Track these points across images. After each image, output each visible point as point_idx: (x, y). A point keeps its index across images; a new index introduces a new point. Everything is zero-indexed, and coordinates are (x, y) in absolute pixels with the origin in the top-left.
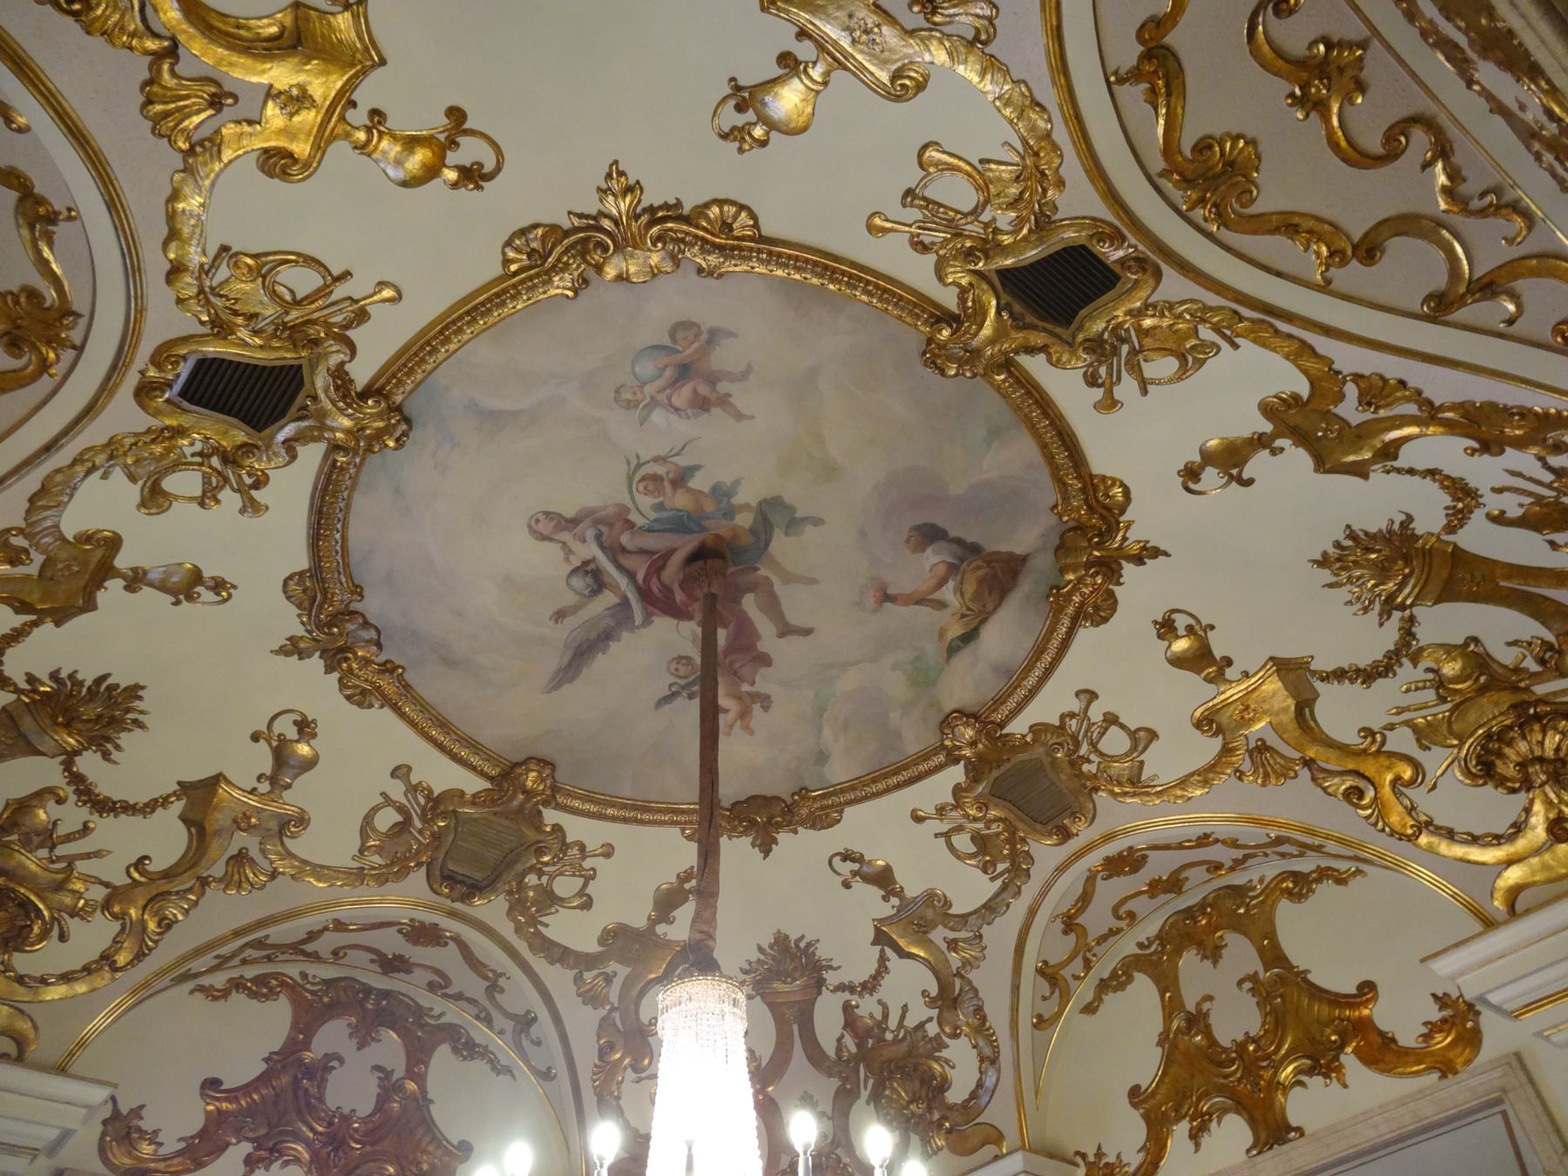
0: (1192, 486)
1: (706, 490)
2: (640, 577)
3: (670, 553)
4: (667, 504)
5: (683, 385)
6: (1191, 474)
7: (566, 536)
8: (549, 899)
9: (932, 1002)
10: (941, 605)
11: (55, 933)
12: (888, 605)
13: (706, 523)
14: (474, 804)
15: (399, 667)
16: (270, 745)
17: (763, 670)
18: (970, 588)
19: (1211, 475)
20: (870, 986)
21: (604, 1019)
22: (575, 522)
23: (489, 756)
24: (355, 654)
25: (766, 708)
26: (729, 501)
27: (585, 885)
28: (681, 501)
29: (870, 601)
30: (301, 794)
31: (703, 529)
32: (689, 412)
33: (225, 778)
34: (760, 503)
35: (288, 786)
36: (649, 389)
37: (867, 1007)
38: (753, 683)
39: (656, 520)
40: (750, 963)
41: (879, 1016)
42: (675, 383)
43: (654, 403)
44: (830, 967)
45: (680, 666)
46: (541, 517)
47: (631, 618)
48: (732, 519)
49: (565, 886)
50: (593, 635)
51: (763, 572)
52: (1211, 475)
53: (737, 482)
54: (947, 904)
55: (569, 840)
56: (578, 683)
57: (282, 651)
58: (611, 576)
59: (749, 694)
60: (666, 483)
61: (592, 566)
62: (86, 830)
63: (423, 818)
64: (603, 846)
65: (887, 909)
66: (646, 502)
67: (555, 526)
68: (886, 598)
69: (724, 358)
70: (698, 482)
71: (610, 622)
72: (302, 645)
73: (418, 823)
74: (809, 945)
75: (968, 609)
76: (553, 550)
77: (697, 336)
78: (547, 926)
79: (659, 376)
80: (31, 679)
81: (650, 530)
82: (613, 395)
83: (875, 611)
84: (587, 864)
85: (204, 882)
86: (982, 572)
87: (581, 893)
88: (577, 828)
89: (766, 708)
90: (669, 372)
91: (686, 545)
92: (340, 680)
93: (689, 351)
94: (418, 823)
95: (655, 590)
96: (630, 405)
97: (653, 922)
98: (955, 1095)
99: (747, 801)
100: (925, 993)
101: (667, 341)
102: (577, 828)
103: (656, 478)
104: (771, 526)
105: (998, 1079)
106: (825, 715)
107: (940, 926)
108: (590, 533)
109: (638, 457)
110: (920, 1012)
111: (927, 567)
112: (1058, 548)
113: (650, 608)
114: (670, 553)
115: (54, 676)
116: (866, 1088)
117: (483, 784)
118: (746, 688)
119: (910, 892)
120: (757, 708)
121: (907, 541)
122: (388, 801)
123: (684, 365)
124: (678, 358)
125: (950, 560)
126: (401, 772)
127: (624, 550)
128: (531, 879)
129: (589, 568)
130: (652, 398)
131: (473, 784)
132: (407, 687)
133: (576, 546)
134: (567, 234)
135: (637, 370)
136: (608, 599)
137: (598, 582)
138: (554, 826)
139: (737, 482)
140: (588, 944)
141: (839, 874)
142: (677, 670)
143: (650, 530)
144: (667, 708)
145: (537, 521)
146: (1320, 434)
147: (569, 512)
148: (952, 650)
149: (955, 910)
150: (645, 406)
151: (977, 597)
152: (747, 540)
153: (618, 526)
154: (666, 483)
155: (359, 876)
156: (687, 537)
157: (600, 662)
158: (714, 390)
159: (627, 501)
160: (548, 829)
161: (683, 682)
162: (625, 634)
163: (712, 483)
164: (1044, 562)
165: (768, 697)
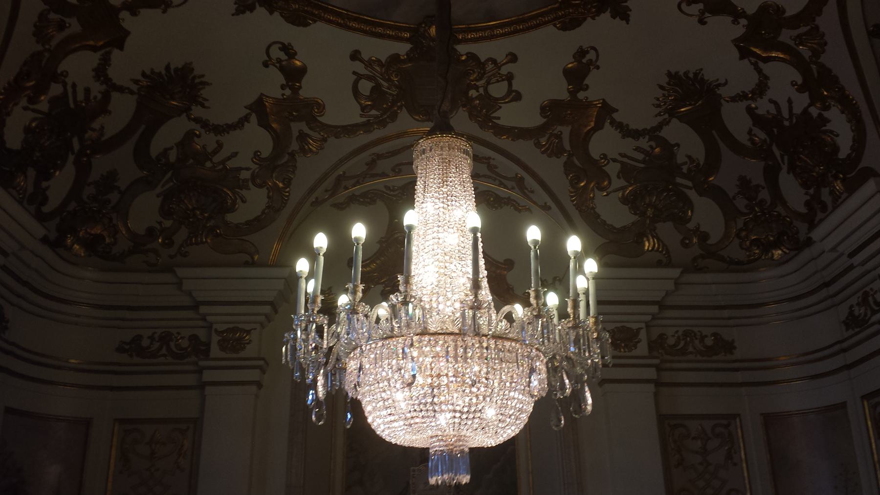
8: (491, 103)
9: (801, 89)
11: (239, 200)
16: (276, 67)
20: (761, 89)
21: (565, 163)
27: (510, 85)
30: (308, 89)
33: (263, 94)
35: (300, 87)
37: (763, 107)
40: (658, 99)
41: (773, 111)
44: (719, 85)
49: (498, 90)
54: (780, 10)
55: (483, 60)
62: (220, 146)
65: (739, 30)
74: (696, 74)
78: (499, 118)
80: (136, 82)
84: (504, 71)
85: (292, 155)
87: (510, 90)
88: (484, 50)
97: (573, 93)
98: (844, 153)
100: (794, 84)
102: (484, 50)
105: (251, 243)
107: (304, 122)
110: (801, 101)
115: (144, 75)
116: (784, 164)
117: (407, 46)
119: (305, 93)
128: (473, 93)
131: (402, 48)
138: (467, 54)
140: (536, 120)
141: (691, 15)
149: (789, 13)
155: (367, 127)
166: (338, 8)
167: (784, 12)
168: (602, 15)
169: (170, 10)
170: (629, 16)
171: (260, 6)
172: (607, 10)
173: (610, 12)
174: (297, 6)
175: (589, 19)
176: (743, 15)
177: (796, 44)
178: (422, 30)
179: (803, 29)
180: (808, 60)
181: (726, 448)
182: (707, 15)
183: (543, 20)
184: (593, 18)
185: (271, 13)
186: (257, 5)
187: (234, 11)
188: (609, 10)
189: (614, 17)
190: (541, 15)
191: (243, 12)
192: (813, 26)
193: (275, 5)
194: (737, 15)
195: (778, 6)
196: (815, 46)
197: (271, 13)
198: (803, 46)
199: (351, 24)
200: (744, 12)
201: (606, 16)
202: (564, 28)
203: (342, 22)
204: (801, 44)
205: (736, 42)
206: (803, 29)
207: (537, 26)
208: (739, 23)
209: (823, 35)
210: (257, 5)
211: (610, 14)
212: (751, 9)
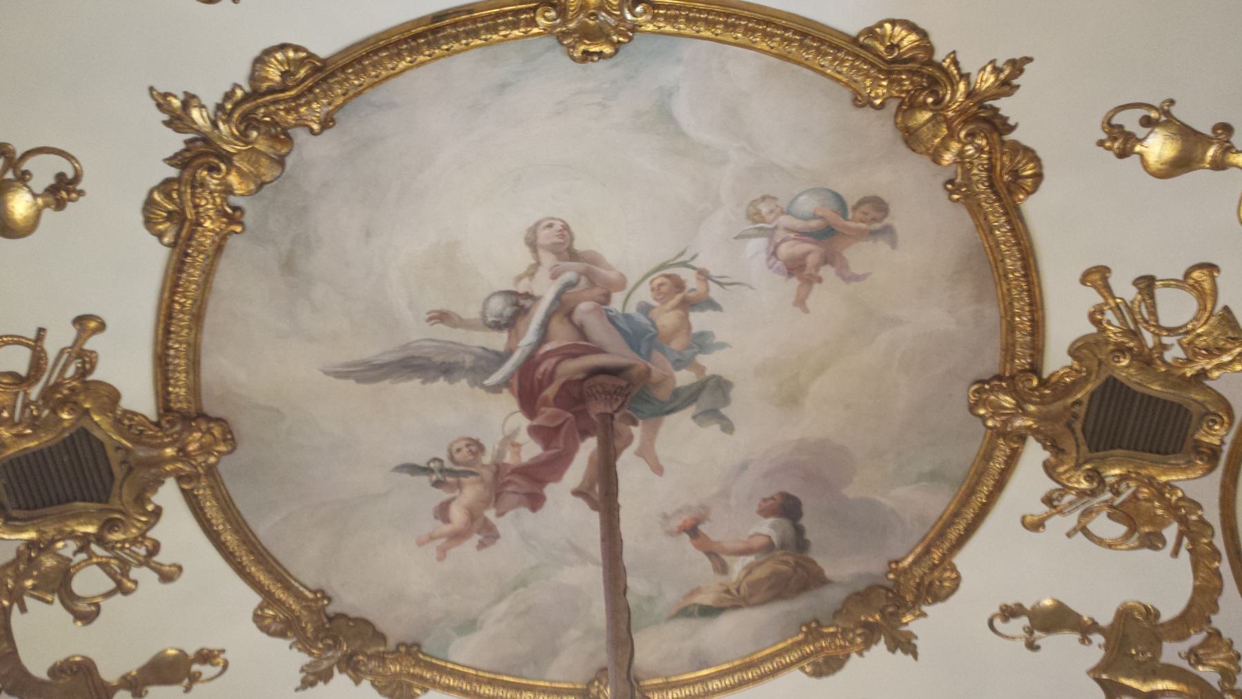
0: (998, 623)
1: (695, 330)
2: (548, 347)
3: (599, 350)
4: (654, 314)
5: (811, 243)
6: (1009, 613)
7: (548, 259)
10: (722, 569)
12: (686, 537)
13: (657, 355)
14: (118, 422)
15: (240, 223)
17: (525, 512)
18: (759, 573)
19: (1018, 625)
22: (573, 255)
23: (195, 390)
24: (228, 173)
25: (482, 545)
26: (695, 354)
28: (667, 319)
29: (676, 523)
31: (648, 357)
32: (779, 264)
34: (714, 376)
36: (785, 220)
38: (500, 515)
39: (627, 317)
42: (803, 235)
43: (770, 233)
45: (465, 450)
46: (558, 225)
47: (489, 373)
48: (678, 369)
50: (439, 359)
51: (636, 431)
52: (1018, 625)
53: (722, 346)
54: (1151, 614)
56: (366, 388)
57: (162, 101)
58: (528, 325)
59: (486, 520)
60: (679, 297)
61: (527, 303)
63: (47, 394)
64: (174, 565)
65: (1095, 651)
66: (645, 294)
67: (555, 244)
68: (693, 531)
69: (858, 255)
70: (699, 320)
71: (469, 360)
72: (195, 113)
73: (35, 392)
75: (738, 590)
76: (524, 258)
77: (874, 220)
79: (806, 219)
81: (612, 320)
82: (758, 196)
83: (670, 533)
86: (784, 568)
89: (482, 545)
90: (814, 224)
91: (617, 353)
92: (168, 181)
93: (852, 224)
94: (35, 392)
95: (542, 369)
96: (754, 216)
99: (356, 620)
101: (851, 203)
103: (679, 285)
104: (695, 400)
106: (522, 590)
108: (569, 276)
109: (693, 258)
111: (751, 532)
112: (858, 594)
113: (515, 382)
114: (599, 350)
118: (490, 514)
120: (476, 538)
121: (765, 500)
122: (36, 344)
123: (833, 230)
124: (838, 221)
125: (775, 540)
126: (86, 324)
127: (569, 315)
129: (522, 302)
130: (776, 228)
132: (219, 249)
133: (543, 275)
134: (931, 63)
135: (802, 198)
136: (498, 341)
137: (512, 320)
139: (722, 346)
141: (1013, 638)
142: (459, 450)
143: (612, 320)
144: (406, 477)
145: (550, 226)
146: (1133, 652)
147: (579, 246)
148: (685, 612)
149: (1167, 614)
150: (760, 229)
151: (754, 586)
152: (663, 394)
153: (597, 292)
154: (679, 297)
156: (627, 351)
157: (412, 387)
158: (817, 267)
159: (631, 283)
160: (150, 508)
161: (448, 464)
162: (464, 383)
163: (707, 329)
164: (833, 596)
165: (497, 536)
166: (463, 666)
167: (1157, 615)
168: (874, 648)
169: (197, 687)
170: (915, 646)
171: (341, 671)
172: (879, 639)
173: (886, 642)
174: (398, 668)
175: (854, 656)
176: (1094, 627)
177: (1190, 664)
178: (594, 691)
179: (1196, 639)
180: (1219, 689)
181: (992, 397)
182: (1037, 633)
183: (783, 661)
184: (860, 654)
185: (357, 682)
186: (336, 670)
187: (298, 684)
188: (883, 639)
189: (892, 649)
190: (779, 653)
191: (313, 684)
192: (1211, 631)
193: (363, 669)
194: (1085, 629)
195: (1146, 607)
196: (1220, 663)
197: (357, 682)
198: (1204, 665)
199: (482, 691)
200: (1095, 623)
201: (880, 648)
202: (818, 672)
203: (468, 688)
204: (1199, 661)
205: (1095, 673)
206: (1196, 639)
207: (774, 673)
208: (1090, 642)
209: (1230, 644)
210: (336, 670)
211: (885, 646)
212: (1105, 618)
